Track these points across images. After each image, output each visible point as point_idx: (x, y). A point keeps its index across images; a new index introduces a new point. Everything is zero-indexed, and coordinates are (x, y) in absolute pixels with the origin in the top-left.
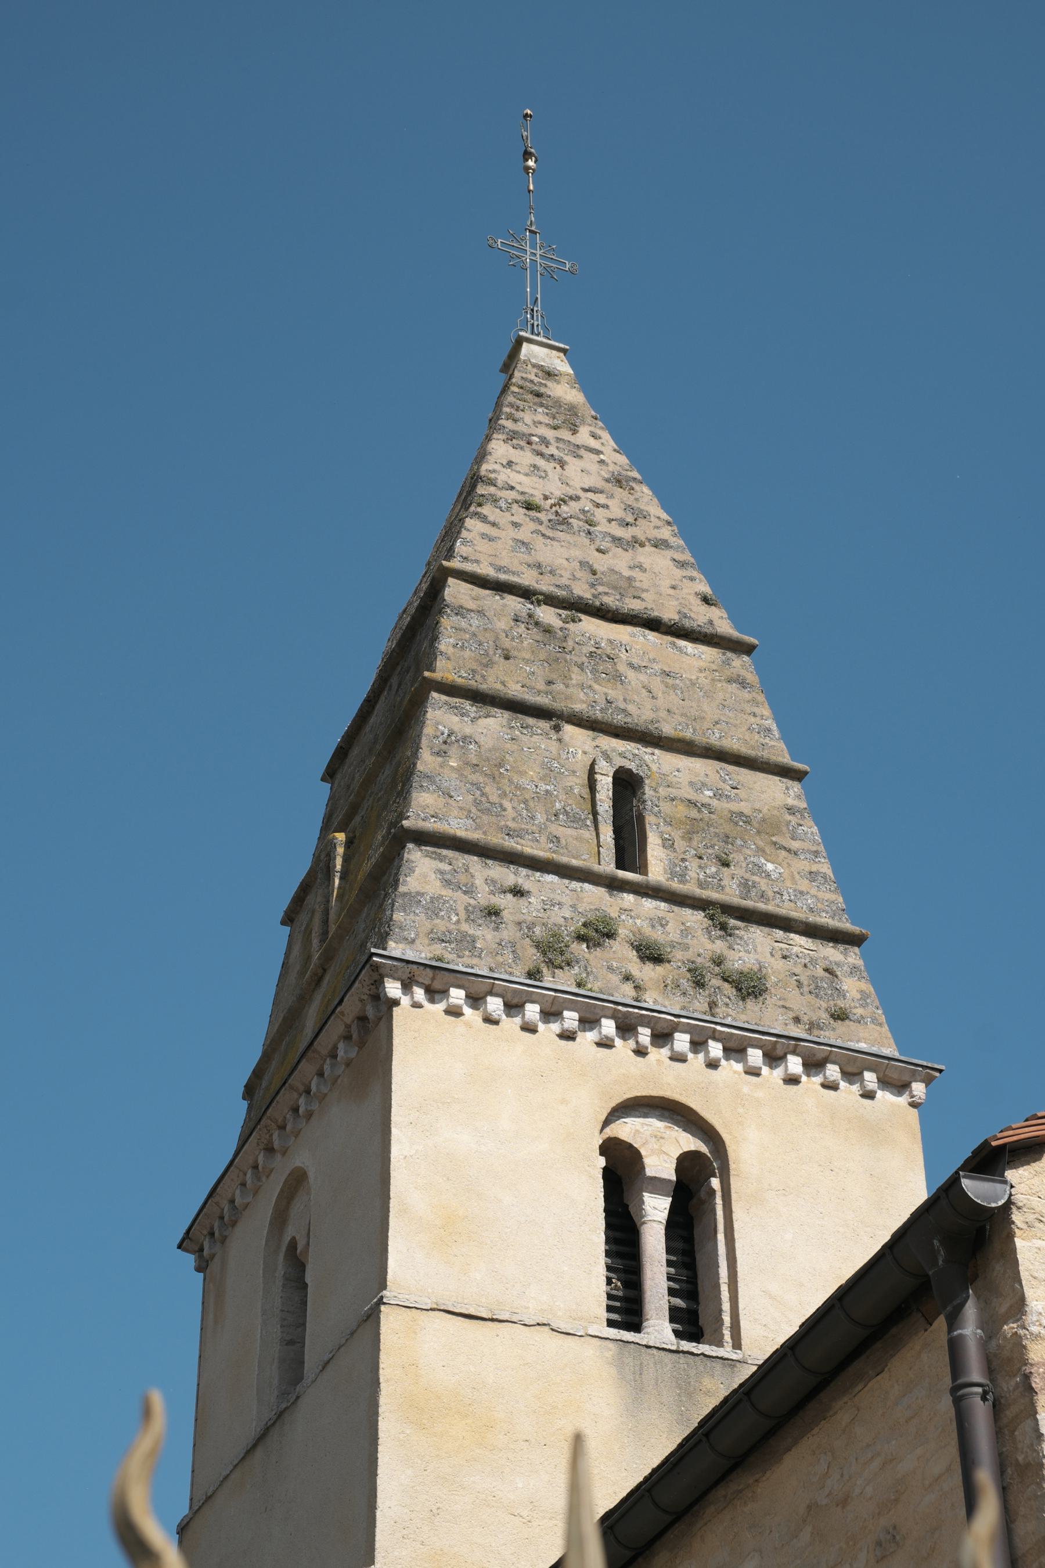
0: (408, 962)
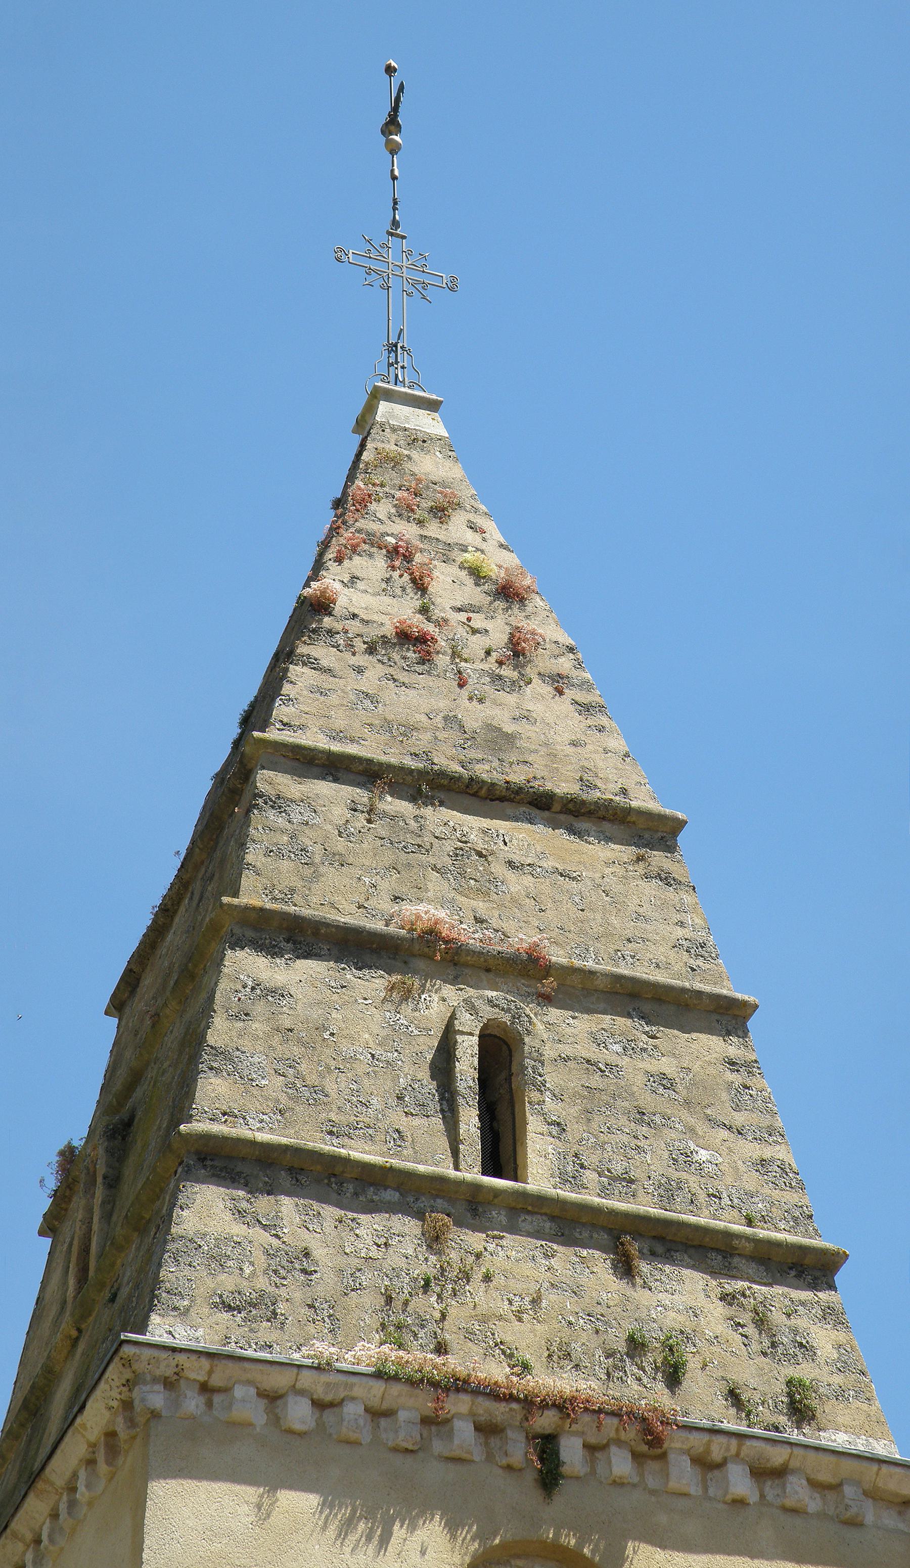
0: (174, 1350)
